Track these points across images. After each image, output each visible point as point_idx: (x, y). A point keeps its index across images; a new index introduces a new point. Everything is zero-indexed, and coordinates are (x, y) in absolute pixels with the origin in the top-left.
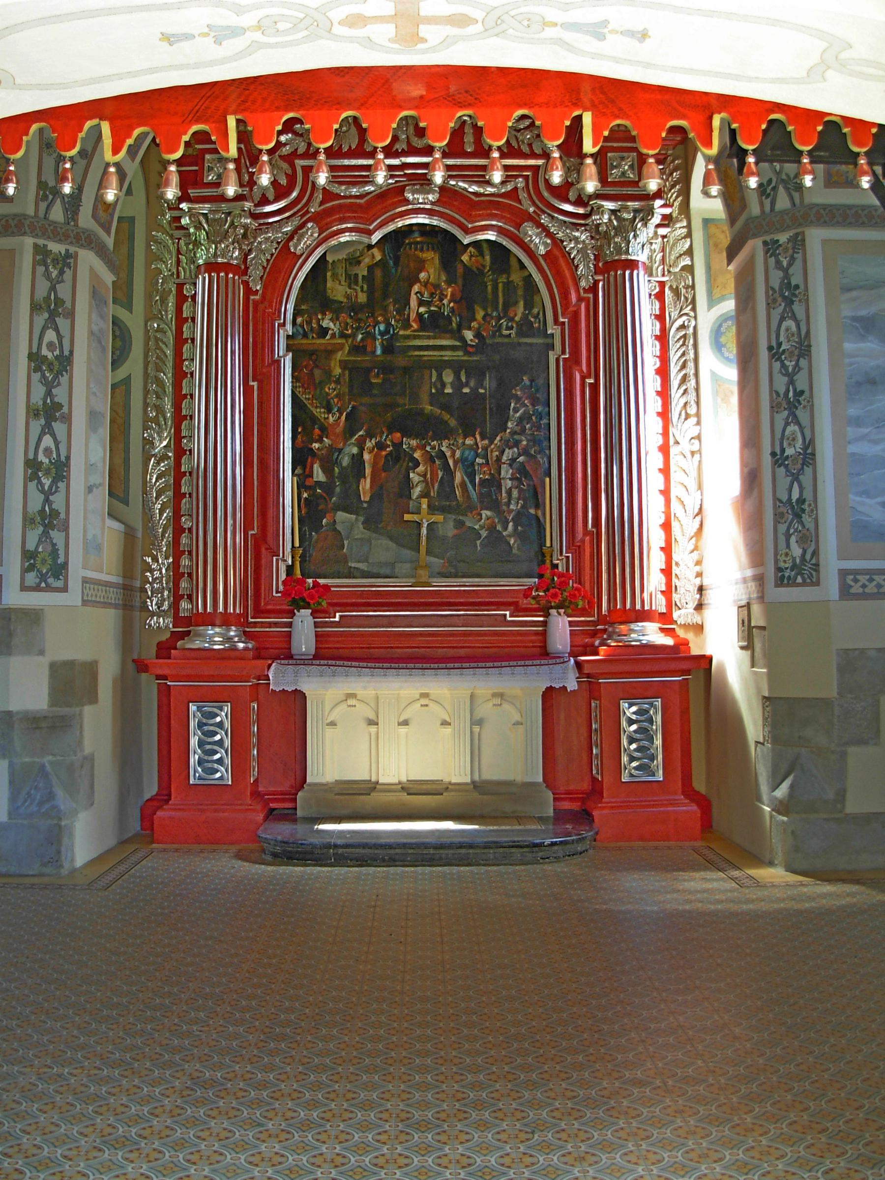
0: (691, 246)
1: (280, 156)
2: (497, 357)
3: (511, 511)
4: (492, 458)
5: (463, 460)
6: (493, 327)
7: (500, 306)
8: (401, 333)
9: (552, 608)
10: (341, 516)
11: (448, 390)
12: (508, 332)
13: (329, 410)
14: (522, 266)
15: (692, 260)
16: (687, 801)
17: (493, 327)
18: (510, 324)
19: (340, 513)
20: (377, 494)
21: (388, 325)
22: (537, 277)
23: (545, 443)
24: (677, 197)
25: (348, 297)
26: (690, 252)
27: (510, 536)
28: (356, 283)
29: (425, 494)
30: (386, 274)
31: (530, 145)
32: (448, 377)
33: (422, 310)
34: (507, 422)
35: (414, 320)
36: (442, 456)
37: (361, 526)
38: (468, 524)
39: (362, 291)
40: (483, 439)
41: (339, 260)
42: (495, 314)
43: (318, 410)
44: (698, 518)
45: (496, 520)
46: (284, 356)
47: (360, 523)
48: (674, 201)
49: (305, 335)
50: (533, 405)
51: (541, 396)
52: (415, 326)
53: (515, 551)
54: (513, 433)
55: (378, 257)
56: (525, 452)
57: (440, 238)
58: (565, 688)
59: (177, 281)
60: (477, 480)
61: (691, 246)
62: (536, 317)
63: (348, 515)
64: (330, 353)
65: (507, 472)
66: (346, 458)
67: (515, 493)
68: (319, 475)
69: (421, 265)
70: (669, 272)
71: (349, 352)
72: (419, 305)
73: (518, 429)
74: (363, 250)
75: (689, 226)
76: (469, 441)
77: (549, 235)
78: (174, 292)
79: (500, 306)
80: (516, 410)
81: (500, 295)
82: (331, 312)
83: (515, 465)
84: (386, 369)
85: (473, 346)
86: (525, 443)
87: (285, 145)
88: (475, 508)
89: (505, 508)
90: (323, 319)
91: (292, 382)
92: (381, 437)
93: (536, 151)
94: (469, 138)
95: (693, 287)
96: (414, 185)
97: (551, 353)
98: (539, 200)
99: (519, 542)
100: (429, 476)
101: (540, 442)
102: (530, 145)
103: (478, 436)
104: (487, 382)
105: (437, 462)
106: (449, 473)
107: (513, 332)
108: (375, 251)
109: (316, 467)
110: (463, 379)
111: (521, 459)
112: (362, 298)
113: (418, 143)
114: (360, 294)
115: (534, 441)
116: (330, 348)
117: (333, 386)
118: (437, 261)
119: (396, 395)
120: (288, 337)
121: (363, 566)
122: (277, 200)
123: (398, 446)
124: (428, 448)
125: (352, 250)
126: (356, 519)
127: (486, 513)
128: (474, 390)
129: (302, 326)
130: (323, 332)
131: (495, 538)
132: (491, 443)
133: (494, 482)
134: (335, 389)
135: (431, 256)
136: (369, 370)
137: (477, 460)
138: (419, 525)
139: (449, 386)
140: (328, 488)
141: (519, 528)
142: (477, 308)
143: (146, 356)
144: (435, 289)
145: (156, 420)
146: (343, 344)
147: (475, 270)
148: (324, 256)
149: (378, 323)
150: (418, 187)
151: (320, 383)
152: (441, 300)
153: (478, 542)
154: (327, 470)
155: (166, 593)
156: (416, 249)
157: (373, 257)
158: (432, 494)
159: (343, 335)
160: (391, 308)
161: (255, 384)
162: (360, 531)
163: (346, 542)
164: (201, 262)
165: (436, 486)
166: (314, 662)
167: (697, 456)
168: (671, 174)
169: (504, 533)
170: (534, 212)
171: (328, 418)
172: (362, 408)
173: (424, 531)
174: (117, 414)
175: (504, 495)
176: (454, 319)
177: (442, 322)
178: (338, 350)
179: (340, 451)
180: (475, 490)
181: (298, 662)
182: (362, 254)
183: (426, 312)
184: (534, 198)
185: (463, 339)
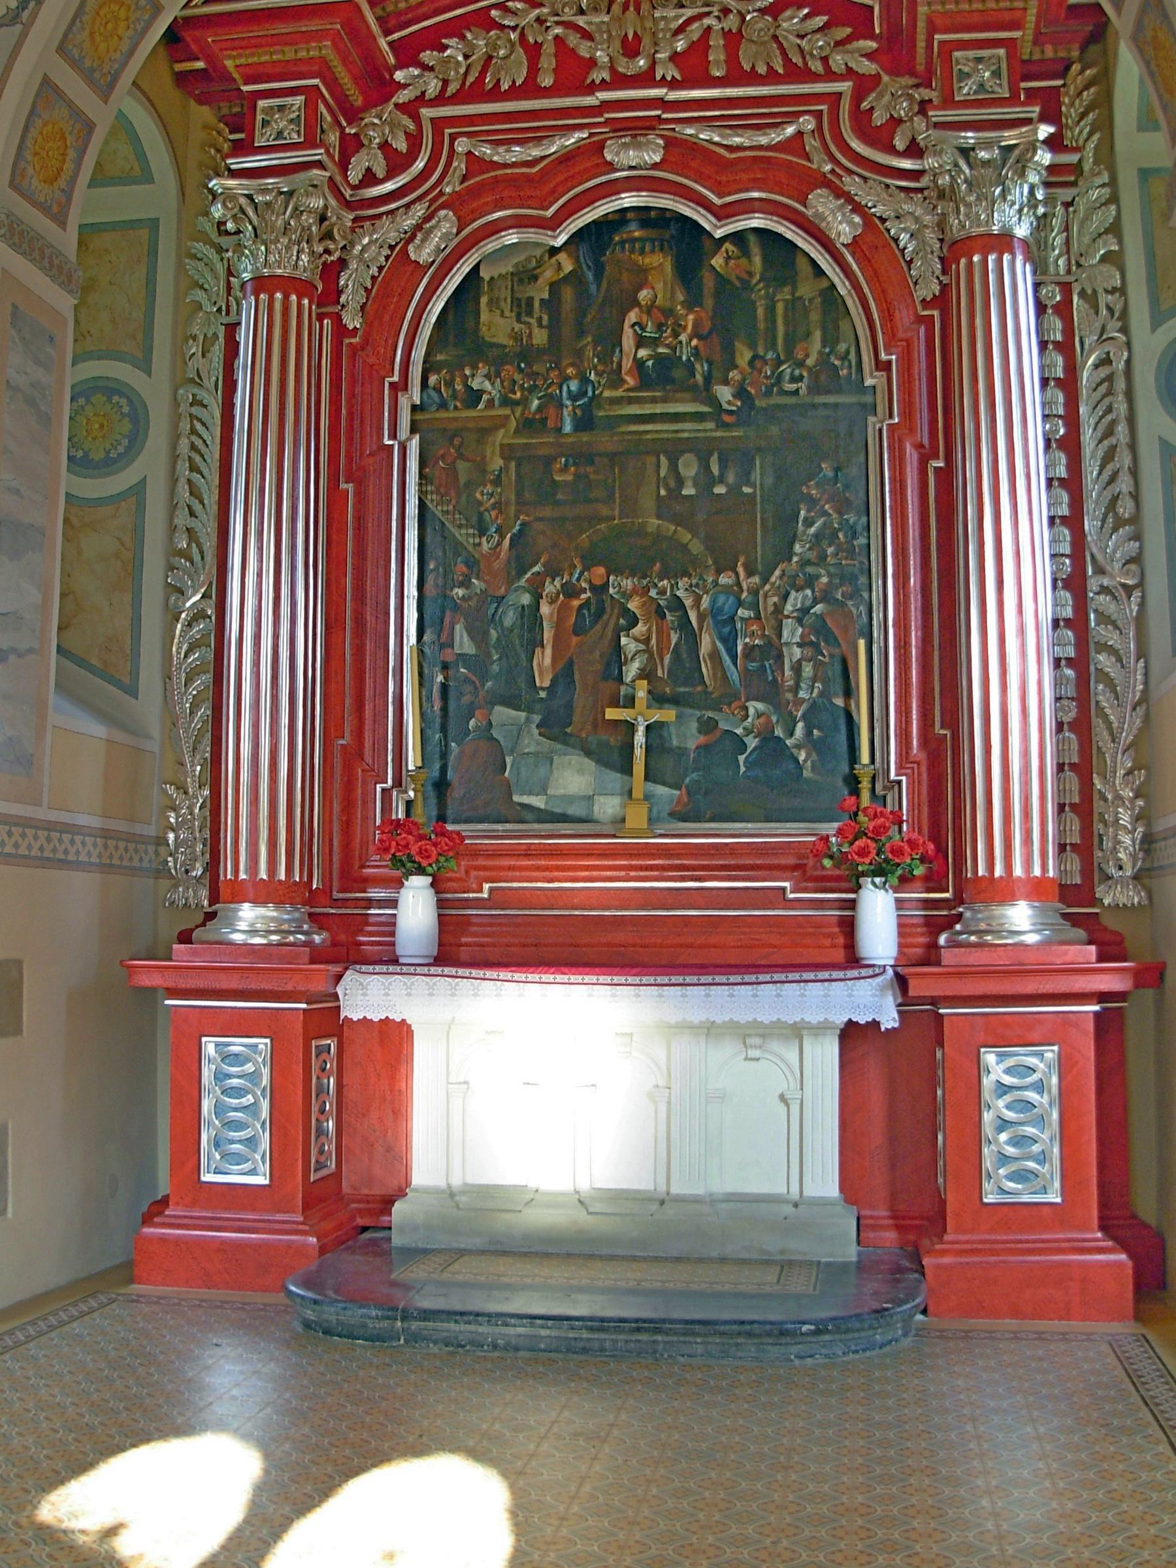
0: (1118, 217)
1: (397, 105)
2: (774, 430)
3: (799, 702)
4: (765, 609)
5: (714, 612)
6: (766, 377)
7: (780, 341)
8: (607, 394)
9: (863, 874)
10: (502, 713)
11: (689, 491)
12: (794, 386)
13: (482, 532)
14: (819, 272)
15: (1120, 242)
16: (1110, 1243)
17: (766, 377)
18: (797, 372)
19: (498, 709)
20: (565, 675)
21: (585, 380)
22: (843, 288)
23: (863, 580)
24: (1090, 134)
25: (517, 337)
26: (1115, 229)
27: (798, 747)
28: (530, 313)
29: (646, 674)
30: (582, 294)
31: (825, 60)
32: (689, 467)
33: (642, 353)
34: (792, 544)
35: (629, 372)
36: (678, 605)
37: (536, 732)
38: (723, 726)
39: (540, 325)
40: (750, 573)
41: (500, 275)
42: (770, 355)
43: (464, 531)
44: (1140, 711)
45: (774, 719)
46: (409, 439)
47: (534, 726)
48: (1086, 140)
49: (443, 405)
50: (841, 514)
51: (857, 499)
52: (631, 381)
53: (807, 773)
54: (805, 563)
55: (568, 267)
56: (826, 596)
57: (673, 230)
58: (875, 1024)
59: (226, 320)
60: (740, 648)
61: (1118, 217)
62: (845, 357)
63: (513, 713)
64: (484, 432)
65: (793, 633)
66: (511, 613)
67: (808, 670)
68: (464, 643)
69: (642, 277)
70: (1079, 265)
71: (517, 431)
72: (638, 346)
73: (812, 555)
74: (542, 256)
75: (1113, 183)
76: (725, 579)
77: (858, 208)
78: (221, 339)
79: (780, 341)
80: (809, 523)
81: (780, 321)
82: (487, 363)
83: (808, 620)
84: (583, 457)
85: (731, 413)
86: (825, 580)
87: (405, 86)
88: (736, 697)
89: (789, 696)
90: (473, 376)
91: (420, 485)
92: (571, 575)
93: (834, 68)
94: (717, 56)
95: (1122, 291)
96: (621, 137)
97: (871, 419)
98: (841, 152)
99: (814, 756)
100: (654, 641)
101: (853, 578)
102: (825, 60)
103: (741, 570)
104: (756, 476)
105: (669, 617)
106: (691, 637)
107: (803, 386)
108: (562, 257)
109: (458, 628)
110: (715, 470)
111: (818, 608)
112: (540, 337)
113: (627, 67)
114: (536, 330)
115: (846, 578)
116: (485, 425)
117: (489, 488)
118: (668, 268)
119: (596, 500)
120: (414, 408)
121: (538, 802)
122: (390, 176)
123: (600, 589)
124: (653, 593)
125: (522, 258)
126: (528, 720)
127: (754, 706)
128: (734, 490)
129: (437, 390)
130: (474, 396)
131: (772, 748)
132: (765, 580)
133: (773, 650)
134: (492, 495)
135: (660, 262)
136: (549, 461)
137: (739, 612)
138: (631, 727)
139: (689, 483)
140: (478, 664)
141: (815, 732)
142: (739, 346)
143: (174, 446)
144: (665, 317)
145: (185, 554)
146: (507, 417)
147: (733, 278)
148: (476, 269)
149: (567, 378)
150: (627, 140)
151: (468, 484)
152: (676, 335)
153: (742, 758)
154: (478, 635)
155: (199, 847)
156: (632, 251)
157: (559, 267)
158: (660, 674)
159: (506, 402)
160: (589, 353)
161: (350, 487)
162: (533, 741)
163: (509, 760)
164: (246, 276)
165: (667, 659)
166: (433, 970)
167: (1137, 594)
168: (1080, 94)
169: (788, 742)
170: (833, 171)
171: (479, 544)
172: (539, 526)
173: (640, 738)
174: (123, 544)
175: (788, 673)
176: (698, 367)
177: (678, 373)
178: (496, 428)
179: (500, 600)
180: (735, 664)
181: (405, 969)
182: (540, 263)
183: (650, 357)
184: (833, 149)
185: (714, 402)
